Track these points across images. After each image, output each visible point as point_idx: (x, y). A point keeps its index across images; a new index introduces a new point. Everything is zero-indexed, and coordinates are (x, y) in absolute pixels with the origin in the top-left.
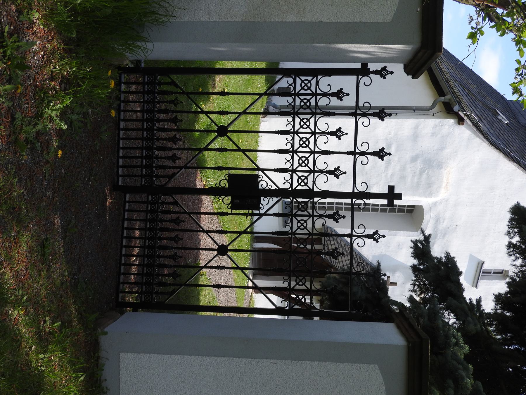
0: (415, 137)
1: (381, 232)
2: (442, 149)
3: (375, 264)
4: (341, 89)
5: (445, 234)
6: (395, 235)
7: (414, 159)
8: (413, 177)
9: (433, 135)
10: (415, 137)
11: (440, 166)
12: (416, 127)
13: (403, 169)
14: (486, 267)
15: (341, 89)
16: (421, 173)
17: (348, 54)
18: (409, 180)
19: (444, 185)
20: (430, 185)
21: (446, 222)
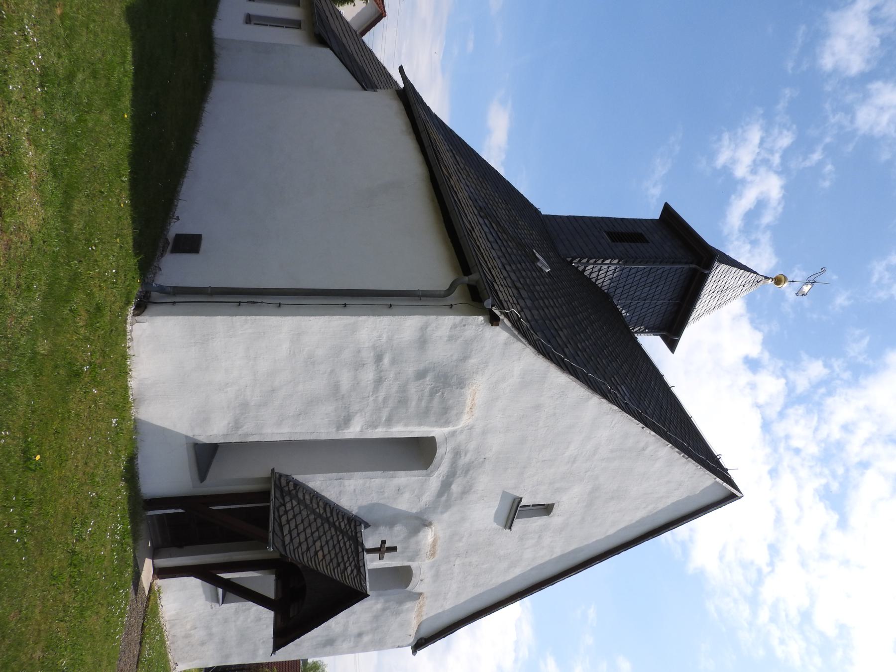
0: (422, 342)
2: (464, 358)
5: (467, 472)
7: (421, 375)
8: (420, 400)
9: (451, 338)
11: (461, 384)
12: (424, 328)
13: (403, 389)
16: (432, 394)
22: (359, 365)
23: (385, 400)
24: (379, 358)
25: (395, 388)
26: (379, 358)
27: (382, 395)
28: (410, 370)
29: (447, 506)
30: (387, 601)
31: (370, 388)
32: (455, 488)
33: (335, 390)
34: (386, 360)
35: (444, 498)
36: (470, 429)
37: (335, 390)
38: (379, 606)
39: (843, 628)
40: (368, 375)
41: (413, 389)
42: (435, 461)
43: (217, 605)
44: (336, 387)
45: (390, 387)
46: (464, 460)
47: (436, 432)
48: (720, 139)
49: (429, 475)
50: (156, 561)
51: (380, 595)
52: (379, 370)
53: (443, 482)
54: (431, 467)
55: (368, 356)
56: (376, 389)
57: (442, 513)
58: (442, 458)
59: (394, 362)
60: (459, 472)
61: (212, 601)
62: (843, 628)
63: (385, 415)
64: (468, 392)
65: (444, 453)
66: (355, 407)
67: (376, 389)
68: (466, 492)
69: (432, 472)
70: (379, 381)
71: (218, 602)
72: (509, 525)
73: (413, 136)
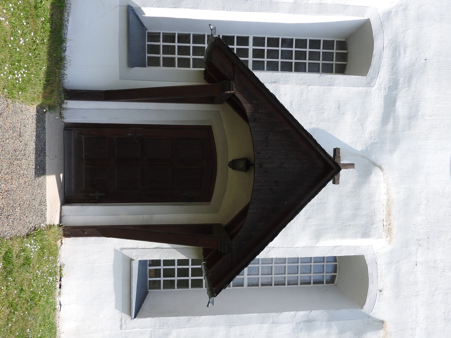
5: (410, 78)
6: (331, 84)
29: (396, 142)
32: (401, 108)
35: (390, 127)
36: (405, 9)
43: (128, 317)
46: (405, 60)
49: (369, 84)
50: (67, 208)
51: (331, 319)
53: (386, 97)
54: (371, 71)
57: (392, 151)
58: (381, 57)
60: (401, 80)
61: (123, 311)
65: (381, 44)
68: (412, 117)
69: (372, 79)
71: (130, 315)
72: (235, 285)
73: (242, 158)
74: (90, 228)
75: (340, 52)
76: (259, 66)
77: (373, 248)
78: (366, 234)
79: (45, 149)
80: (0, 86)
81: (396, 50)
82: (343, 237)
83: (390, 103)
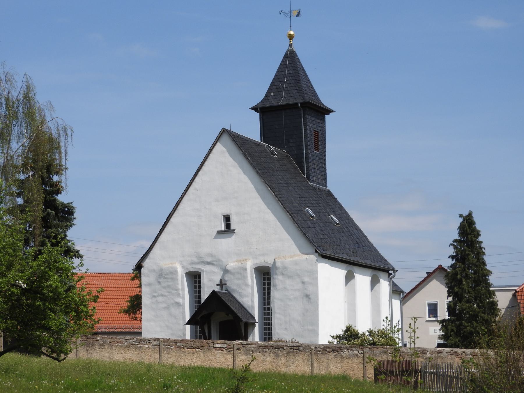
0: (149, 285)
1: (219, 287)
2: (154, 271)
3: (461, 220)
4: (329, 111)
5: (200, 257)
6: (204, 284)
7: (159, 283)
8: (168, 282)
9: (148, 276)
10: (149, 285)
11: (161, 270)
12: (145, 285)
13: (164, 288)
14: (223, 228)
15: (329, 111)
16: (165, 278)
17: (202, 302)
18: (170, 283)
19: (171, 265)
20: (171, 273)
21: (193, 259)
22: (157, 302)
23: (169, 292)
24: (154, 297)
25: (164, 290)
26: (154, 297)
27: (167, 294)
28: (158, 287)
29: (219, 260)
30: (276, 274)
31: (165, 298)
32: (209, 260)
33: (167, 308)
34: (155, 294)
35: (215, 263)
37: (167, 308)
38: (280, 277)
39: (234, 230)
40: (160, 299)
41: (164, 284)
42: (196, 270)
44: (165, 308)
45: (164, 291)
46: (196, 260)
47: (181, 272)
48: (443, 331)
52: (159, 296)
55: (154, 300)
56: (165, 296)
57: (222, 262)
59: (156, 292)
62: (234, 230)
63: (174, 292)
64: (164, 267)
65: (192, 268)
66: (172, 301)
67: (165, 296)
68: (211, 255)
69: (202, 270)
70: (162, 295)
74: (416, 287)
75: (195, 278)
76: (200, 301)
77: (250, 265)
78: (245, 269)
79: (185, 312)
80: (198, 392)
81: (193, 263)
82: (247, 277)
83: (208, 263)
